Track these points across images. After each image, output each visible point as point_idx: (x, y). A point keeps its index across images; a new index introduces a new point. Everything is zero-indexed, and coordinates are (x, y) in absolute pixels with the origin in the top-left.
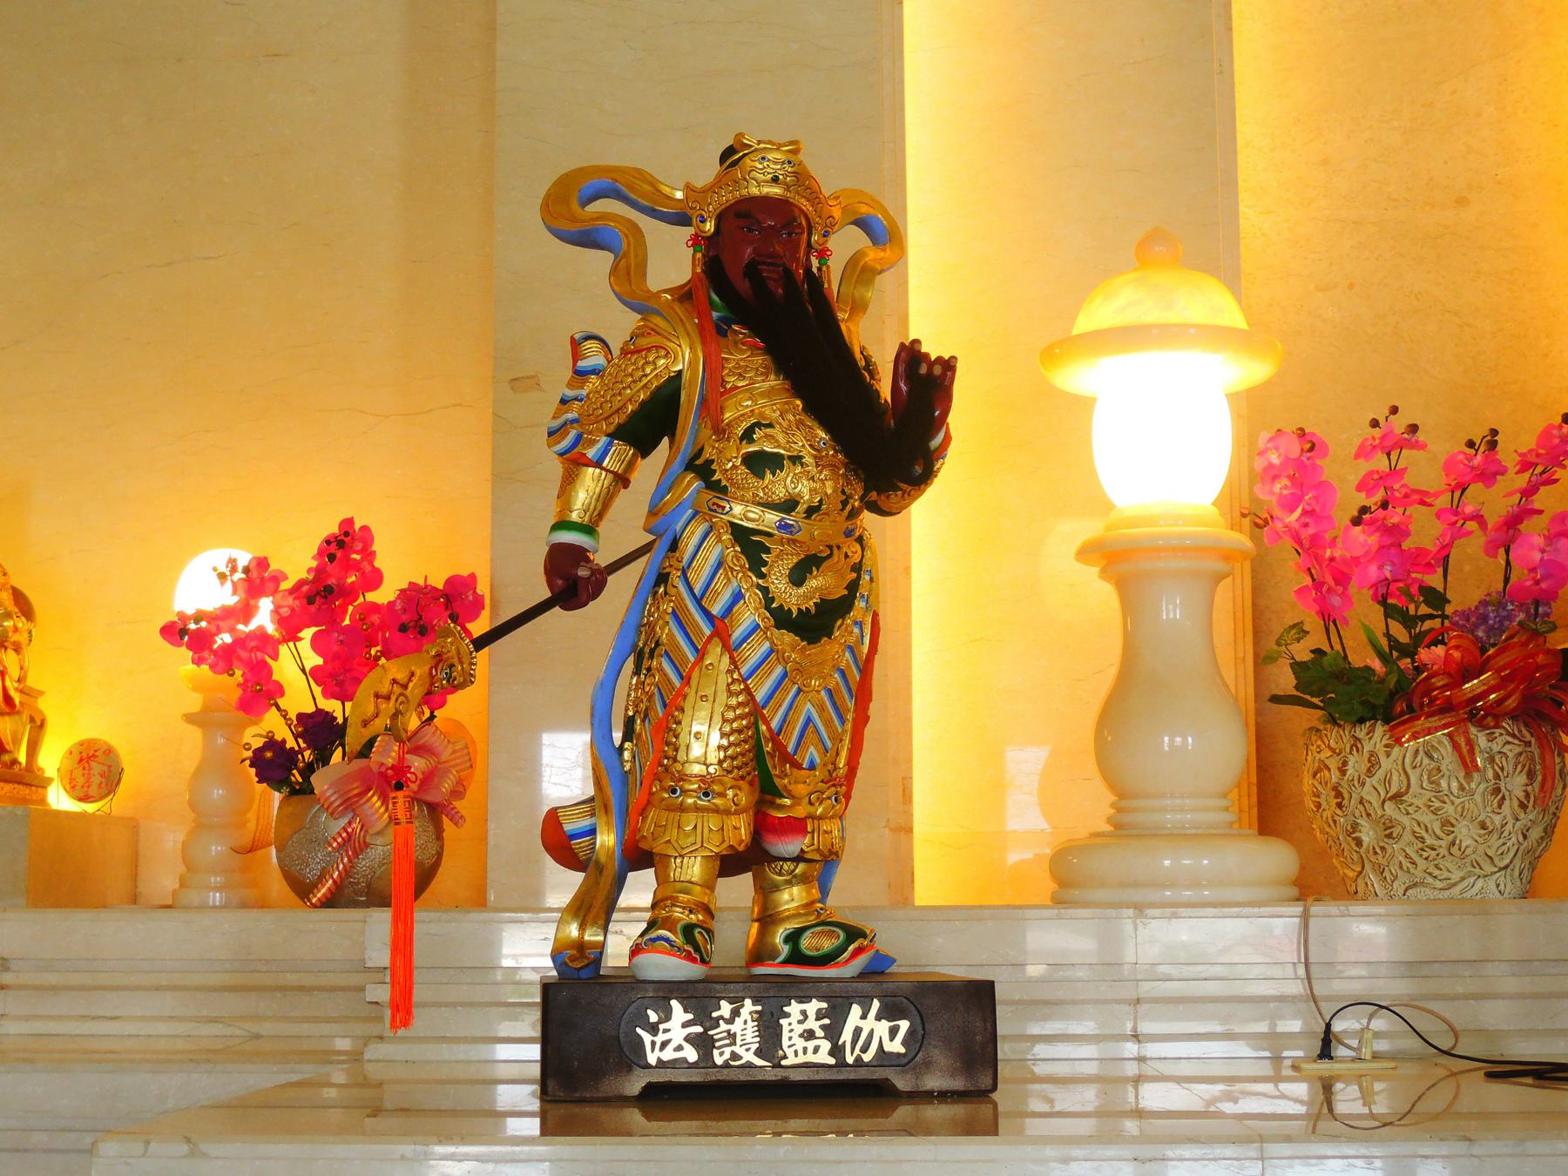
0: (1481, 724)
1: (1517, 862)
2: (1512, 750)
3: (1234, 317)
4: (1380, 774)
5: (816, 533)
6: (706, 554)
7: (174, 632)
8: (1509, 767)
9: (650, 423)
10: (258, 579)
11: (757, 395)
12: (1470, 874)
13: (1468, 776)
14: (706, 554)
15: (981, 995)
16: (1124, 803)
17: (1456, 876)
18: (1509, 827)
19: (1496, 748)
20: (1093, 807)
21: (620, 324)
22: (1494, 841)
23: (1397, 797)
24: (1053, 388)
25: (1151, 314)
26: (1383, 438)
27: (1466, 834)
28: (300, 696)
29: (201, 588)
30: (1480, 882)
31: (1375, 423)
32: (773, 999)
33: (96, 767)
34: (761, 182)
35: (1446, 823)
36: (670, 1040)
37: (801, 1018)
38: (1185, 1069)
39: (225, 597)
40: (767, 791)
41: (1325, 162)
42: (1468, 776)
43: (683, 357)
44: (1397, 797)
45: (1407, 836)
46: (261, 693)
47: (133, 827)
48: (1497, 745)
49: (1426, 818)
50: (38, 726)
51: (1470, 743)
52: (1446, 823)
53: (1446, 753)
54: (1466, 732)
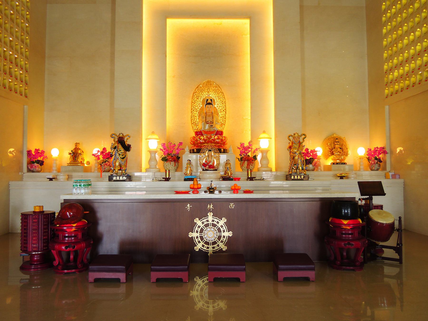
5: (123, 154)
6: (117, 154)
7: (93, 155)
9: (115, 148)
10: (98, 151)
11: (120, 147)
14: (117, 154)
15: (130, 176)
20: (148, 167)
21: (114, 143)
25: (151, 137)
28: (101, 159)
29: (95, 152)
32: (120, 176)
33: (88, 163)
34: (121, 135)
36: (114, 178)
37: (121, 177)
38: (274, 192)
39: (97, 152)
40: (121, 167)
43: (116, 145)
46: (99, 159)
47: (91, 167)
48: (173, 163)
50: (84, 160)
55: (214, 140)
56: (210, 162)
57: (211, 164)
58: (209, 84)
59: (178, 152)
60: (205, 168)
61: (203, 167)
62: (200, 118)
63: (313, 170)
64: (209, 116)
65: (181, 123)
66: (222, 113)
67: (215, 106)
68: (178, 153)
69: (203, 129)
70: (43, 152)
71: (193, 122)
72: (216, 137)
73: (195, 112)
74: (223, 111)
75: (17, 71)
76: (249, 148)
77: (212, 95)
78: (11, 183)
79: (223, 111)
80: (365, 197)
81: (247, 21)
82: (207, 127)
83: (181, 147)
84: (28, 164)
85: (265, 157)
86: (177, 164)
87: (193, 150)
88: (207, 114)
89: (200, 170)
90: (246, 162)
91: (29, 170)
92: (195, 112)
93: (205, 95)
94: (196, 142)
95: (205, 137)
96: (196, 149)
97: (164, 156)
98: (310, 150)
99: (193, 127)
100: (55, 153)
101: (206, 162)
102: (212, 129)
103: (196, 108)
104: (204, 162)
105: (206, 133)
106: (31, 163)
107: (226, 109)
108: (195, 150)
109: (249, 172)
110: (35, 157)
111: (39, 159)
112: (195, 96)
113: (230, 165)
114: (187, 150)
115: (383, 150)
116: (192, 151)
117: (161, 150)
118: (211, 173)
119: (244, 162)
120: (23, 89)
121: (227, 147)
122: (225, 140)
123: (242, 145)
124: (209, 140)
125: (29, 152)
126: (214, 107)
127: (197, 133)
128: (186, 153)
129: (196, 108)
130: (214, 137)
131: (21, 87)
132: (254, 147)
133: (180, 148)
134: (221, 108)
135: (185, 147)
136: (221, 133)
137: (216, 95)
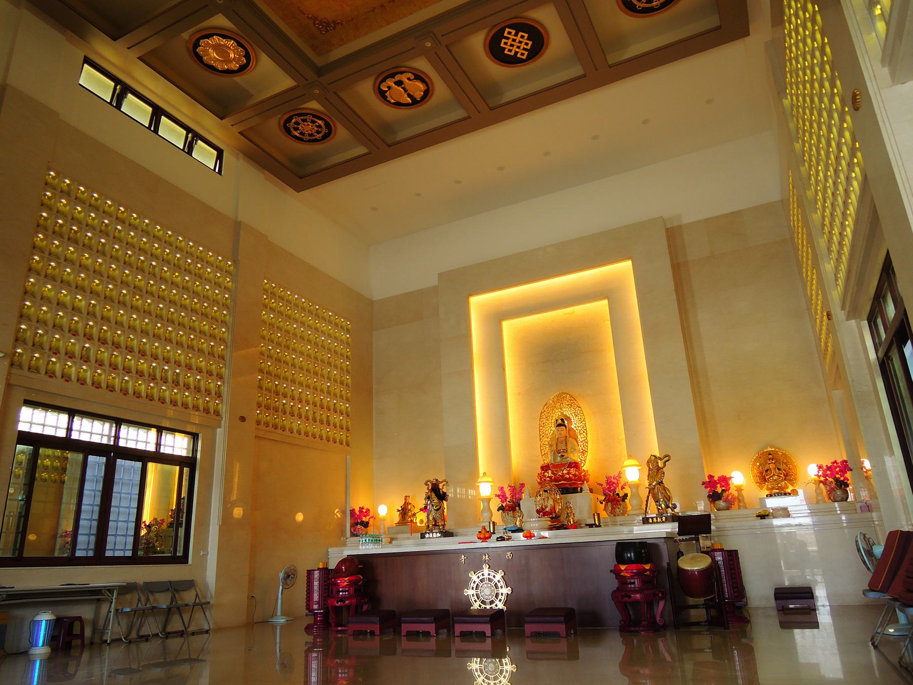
3: (490, 480)
58: (560, 397)
63: (728, 508)
64: (562, 442)
65: (525, 455)
70: (368, 510)
75: (336, 418)
77: (567, 412)
78: (330, 550)
80: (684, 537)
81: (606, 302)
84: (351, 526)
85: (636, 495)
90: (57, 464)
91: (353, 535)
93: (557, 414)
98: (716, 478)
100: (383, 511)
102: (564, 461)
106: (354, 525)
110: (360, 517)
111: (364, 519)
115: (845, 467)
117: (497, 496)
120: (344, 437)
124: (562, 478)
125: (353, 512)
127: (542, 468)
131: (340, 435)
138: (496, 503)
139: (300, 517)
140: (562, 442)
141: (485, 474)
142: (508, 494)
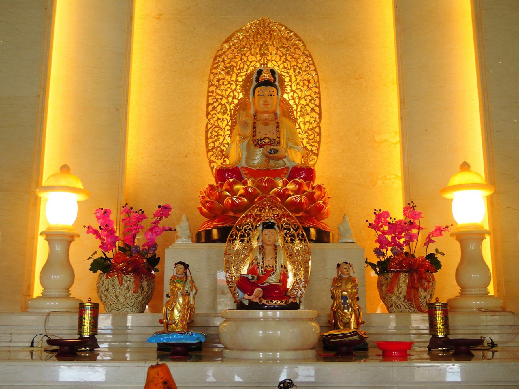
0: (124, 274)
1: (135, 304)
2: (133, 280)
3: (80, 186)
4: (104, 285)
8: (131, 284)
12: (123, 307)
13: (121, 286)
16: (46, 290)
17: (120, 308)
18: (131, 297)
19: (128, 279)
22: (128, 300)
23: (107, 290)
24: (444, 198)
26: (125, 210)
27: (121, 299)
30: (126, 309)
31: (123, 207)
35: (116, 296)
41: (156, 147)
42: (121, 286)
44: (107, 290)
45: (109, 299)
48: (129, 279)
49: (112, 295)
51: (122, 278)
52: (116, 296)
53: (117, 281)
54: (121, 276)
55: (283, 196)
56: (269, 272)
57: (273, 279)
59: (152, 240)
60: (246, 299)
61: (240, 294)
62: (237, 128)
64: (266, 122)
66: (307, 118)
67: (285, 96)
68: (152, 245)
69: (244, 164)
71: (211, 146)
72: (291, 187)
73: (220, 116)
74: (313, 110)
76: (412, 225)
79: (313, 110)
82: (258, 158)
83: (164, 222)
85: (470, 259)
86: (145, 283)
87: (208, 233)
88: (259, 116)
89: (226, 304)
90: (403, 279)
92: (220, 116)
93: (253, 64)
94: (218, 205)
95: (249, 184)
96: (219, 230)
97: (100, 254)
99: (211, 162)
101: (251, 271)
102: (275, 165)
103: (224, 101)
104: (245, 270)
105: (255, 173)
107: (320, 106)
108: (215, 232)
109: (439, 319)
112: (222, 65)
113: (355, 287)
114: (183, 230)
116: (203, 237)
117: (90, 230)
118: (274, 319)
119: (395, 279)
121: (329, 223)
122: (321, 197)
123: (381, 216)
126: (284, 101)
127: (221, 174)
128: (179, 241)
129: (224, 101)
130: (285, 184)
132: (428, 223)
133: (161, 225)
134: (303, 102)
135: (179, 220)
136: (309, 173)
137: (288, 65)
138: (86, 249)
139: (237, 379)
140: (266, 122)
141: (65, 169)
142: (119, 230)
